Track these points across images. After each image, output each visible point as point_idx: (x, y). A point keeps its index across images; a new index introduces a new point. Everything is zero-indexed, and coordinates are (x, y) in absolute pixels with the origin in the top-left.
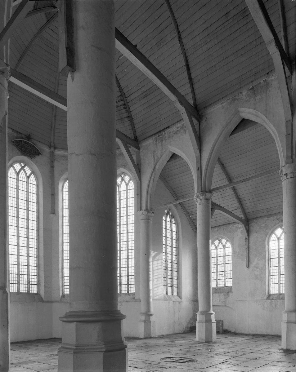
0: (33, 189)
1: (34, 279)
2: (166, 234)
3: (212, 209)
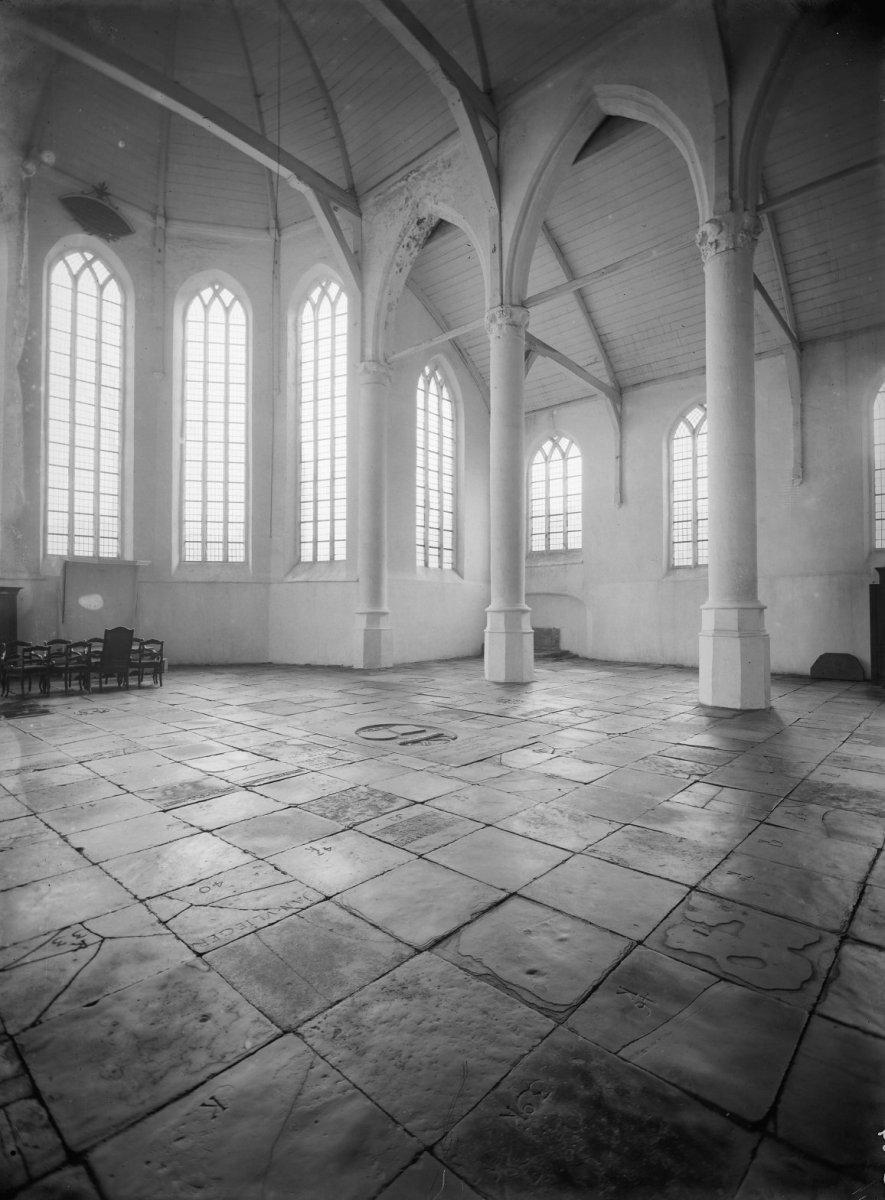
0: (113, 314)
1: (237, 532)
2: (426, 424)
3: (527, 353)
